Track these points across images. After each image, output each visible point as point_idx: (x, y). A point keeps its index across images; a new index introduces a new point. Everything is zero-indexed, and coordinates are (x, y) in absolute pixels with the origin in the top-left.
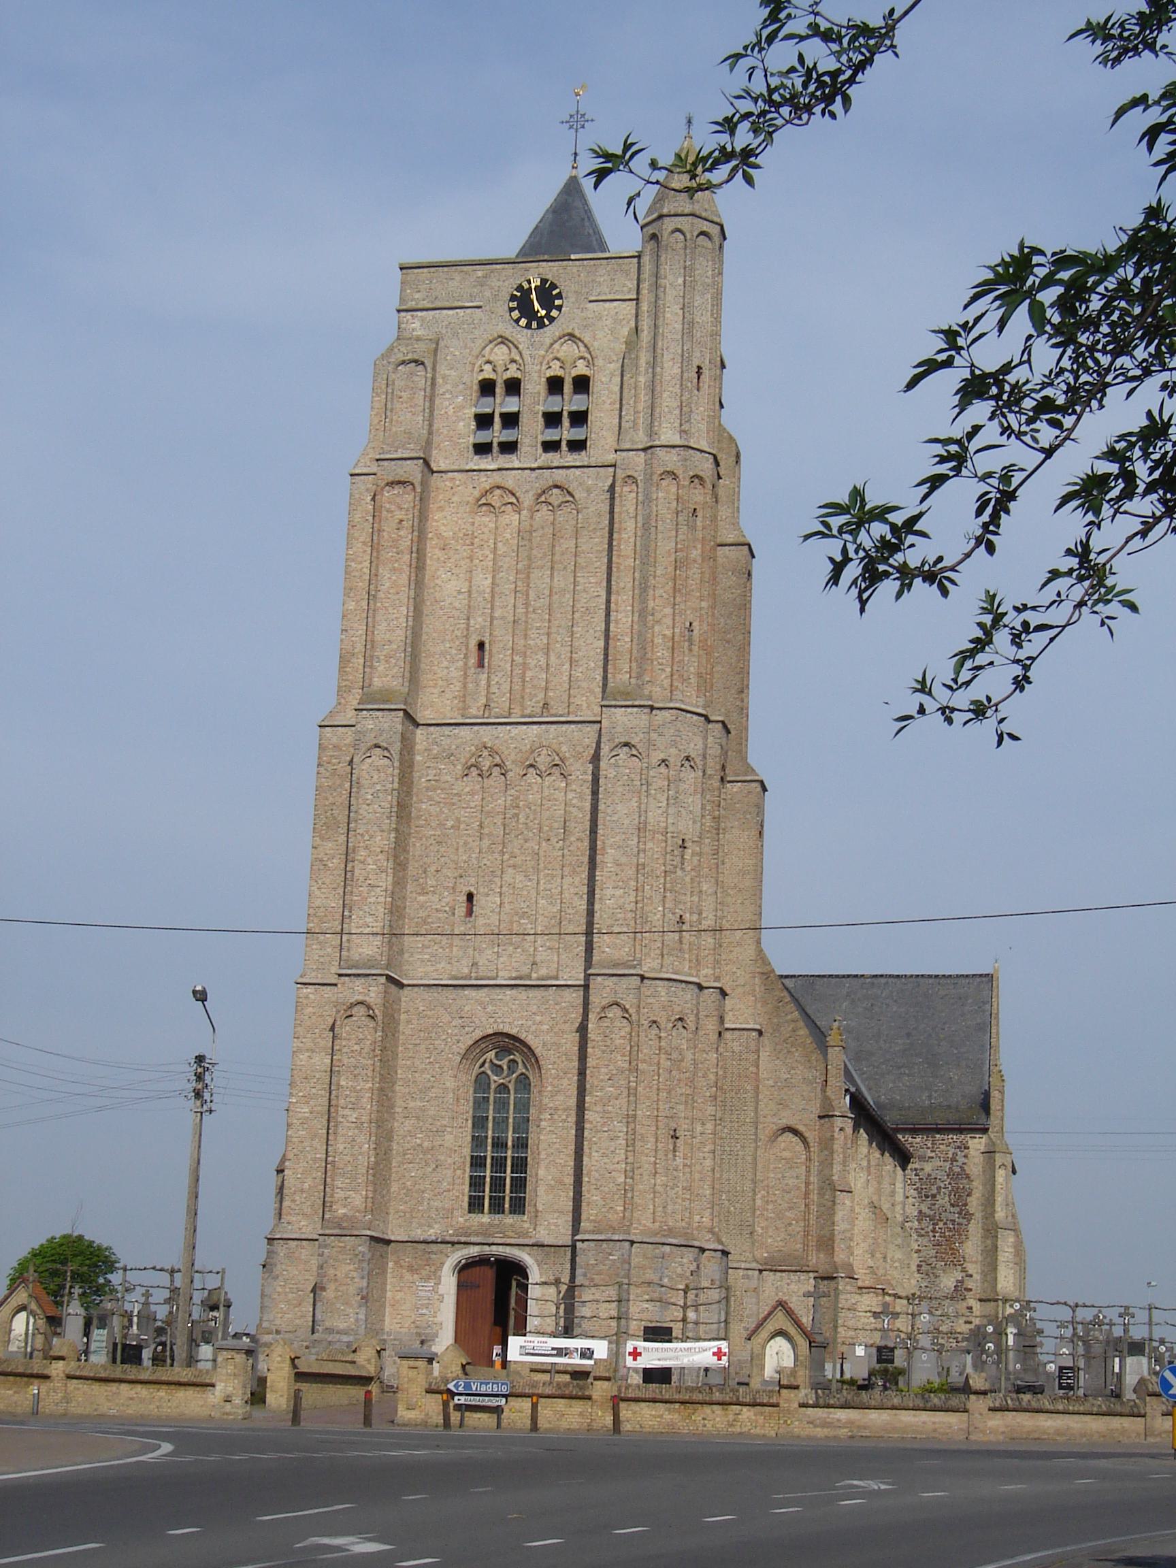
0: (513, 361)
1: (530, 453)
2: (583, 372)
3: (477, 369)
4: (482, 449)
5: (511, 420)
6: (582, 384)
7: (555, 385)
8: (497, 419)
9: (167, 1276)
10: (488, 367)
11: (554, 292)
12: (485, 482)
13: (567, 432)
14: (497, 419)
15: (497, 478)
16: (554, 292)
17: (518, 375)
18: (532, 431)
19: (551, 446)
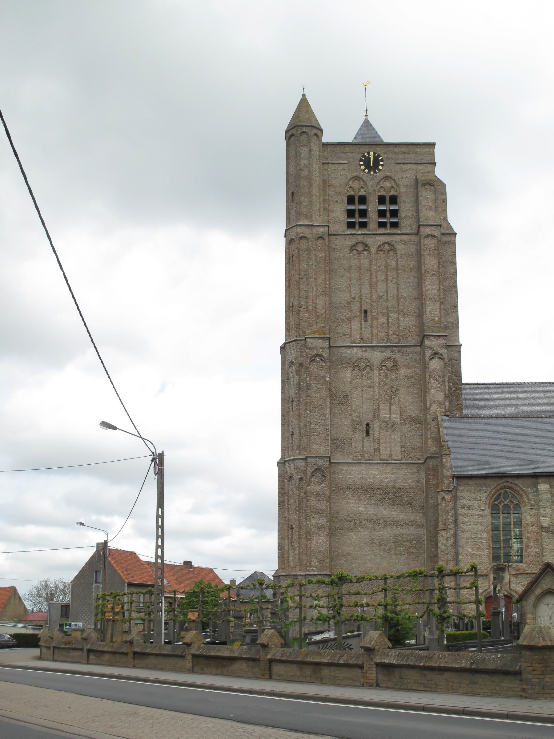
0: (362, 187)
1: (373, 228)
2: (394, 194)
3: (377, 190)
4: (351, 225)
5: (363, 213)
6: (394, 200)
7: (381, 200)
8: (388, 213)
9: (381, 582)
10: (382, 190)
11: (380, 159)
12: (354, 239)
13: (357, 219)
14: (388, 213)
15: (360, 238)
16: (380, 159)
17: (396, 194)
18: (373, 218)
19: (382, 225)
